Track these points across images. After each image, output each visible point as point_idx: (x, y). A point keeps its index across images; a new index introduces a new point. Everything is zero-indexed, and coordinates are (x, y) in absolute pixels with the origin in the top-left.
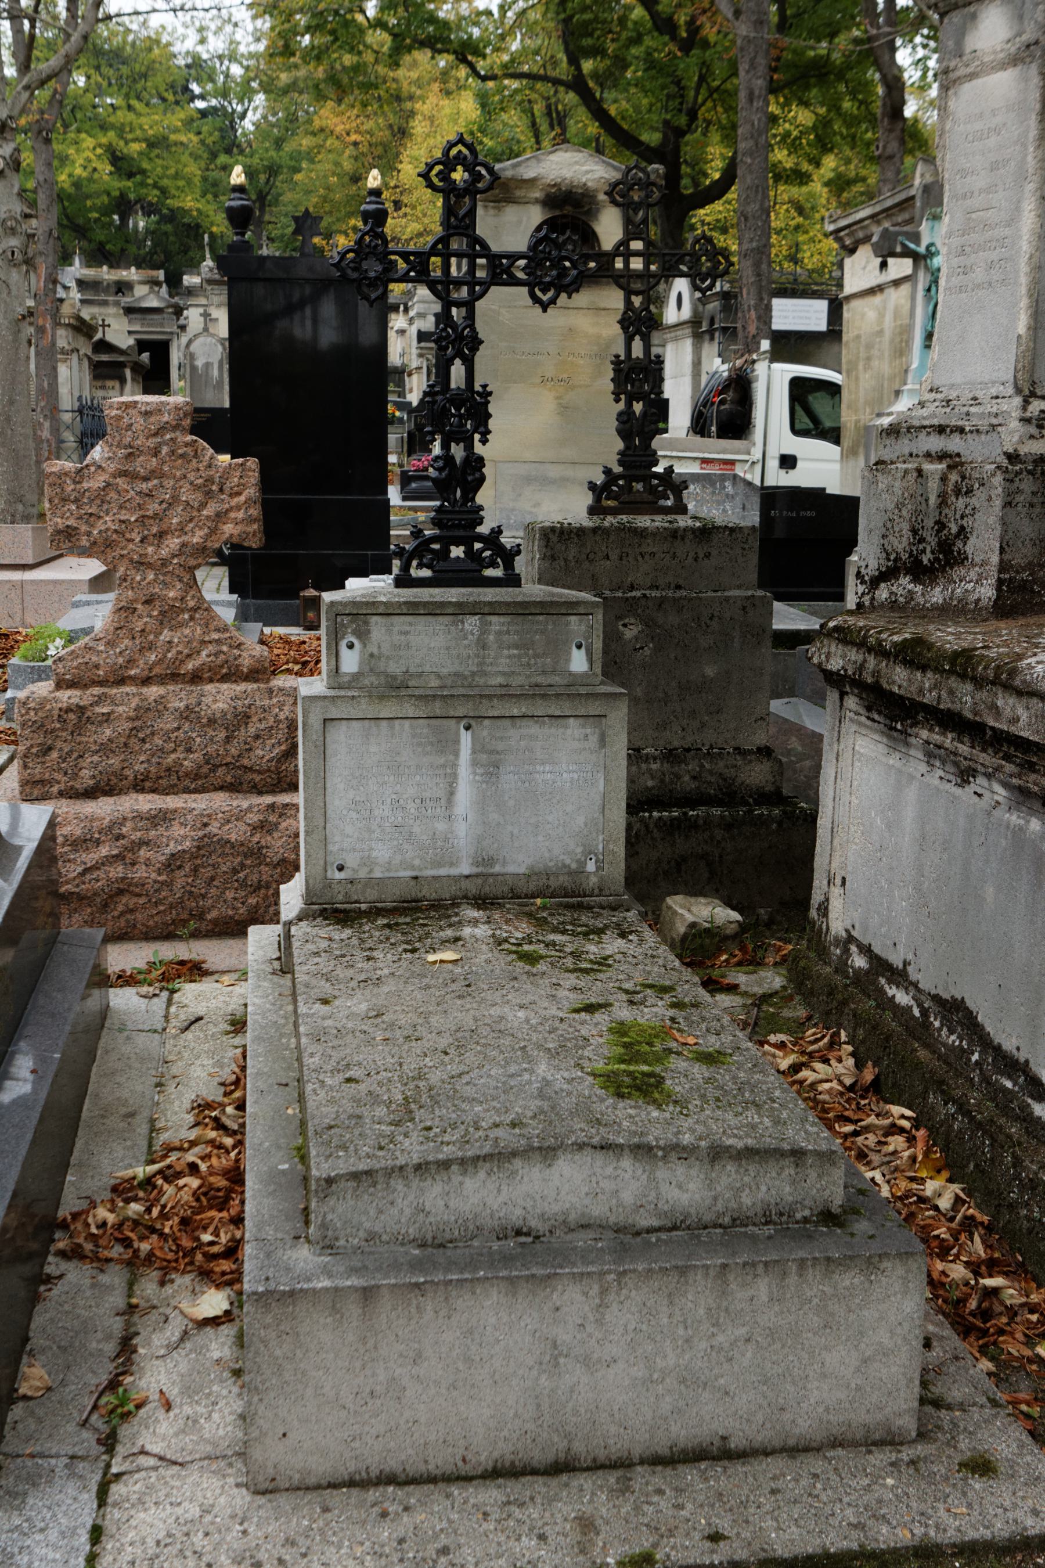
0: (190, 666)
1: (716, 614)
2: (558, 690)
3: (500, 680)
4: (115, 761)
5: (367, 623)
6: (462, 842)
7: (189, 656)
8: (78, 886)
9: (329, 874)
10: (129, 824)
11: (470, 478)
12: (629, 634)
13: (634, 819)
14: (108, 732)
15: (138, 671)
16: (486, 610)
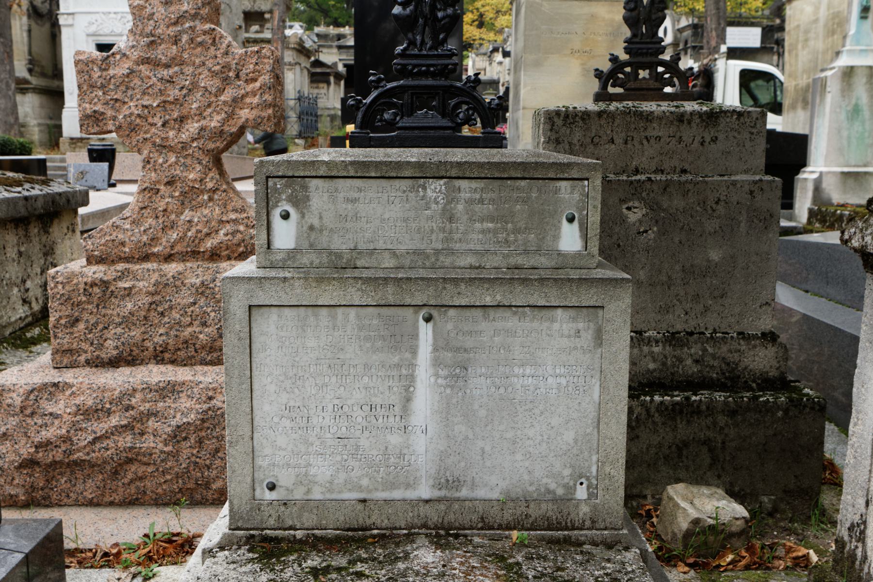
0: (209, 245)
1: (723, 198)
2: (544, 274)
3: (470, 260)
4: (136, 333)
5: (305, 188)
6: (421, 460)
7: (208, 235)
8: (88, 454)
9: (258, 493)
10: (139, 396)
11: (440, 14)
12: (633, 217)
13: (635, 403)
14: (129, 306)
15: (161, 248)
16: (453, 173)
